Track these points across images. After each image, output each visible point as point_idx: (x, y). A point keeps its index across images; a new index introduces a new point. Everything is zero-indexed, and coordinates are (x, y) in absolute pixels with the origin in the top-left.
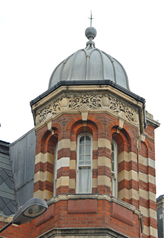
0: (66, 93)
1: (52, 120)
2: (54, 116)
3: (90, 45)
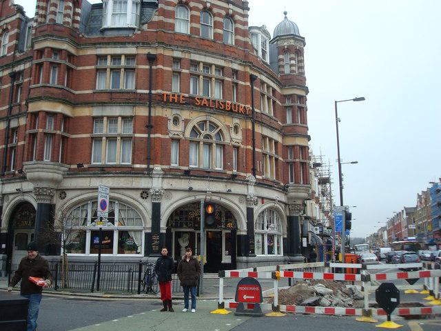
0: (293, 38)
3: (286, 18)
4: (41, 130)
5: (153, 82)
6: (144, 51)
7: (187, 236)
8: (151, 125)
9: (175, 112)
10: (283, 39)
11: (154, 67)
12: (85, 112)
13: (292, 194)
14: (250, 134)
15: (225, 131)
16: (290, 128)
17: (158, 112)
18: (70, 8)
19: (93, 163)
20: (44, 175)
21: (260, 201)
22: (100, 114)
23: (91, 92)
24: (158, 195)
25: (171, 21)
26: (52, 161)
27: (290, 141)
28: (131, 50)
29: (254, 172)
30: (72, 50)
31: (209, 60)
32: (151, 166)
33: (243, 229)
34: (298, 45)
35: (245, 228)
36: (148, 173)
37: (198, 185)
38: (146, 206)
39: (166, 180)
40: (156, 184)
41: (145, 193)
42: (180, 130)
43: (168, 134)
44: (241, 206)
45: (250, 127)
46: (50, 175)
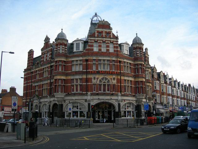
4: (57, 84)
8: (87, 80)
9: (94, 76)
11: (88, 63)
12: (70, 77)
13: (138, 97)
14: (119, 80)
15: (110, 80)
18: (63, 48)
19: (72, 92)
20: (59, 96)
21: (123, 101)
22: (73, 78)
24: (89, 101)
25: (92, 48)
26: (61, 92)
27: (137, 80)
28: (81, 58)
29: (121, 92)
30: (65, 60)
31: (105, 58)
32: (87, 93)
33: (117, 110)
34: (140, 46)
35: (118, 109)
36: (86, 94)
37: (101, 97)
38: (86, 104)
39: (92, 97)
40: (89, 98)
41: (86, 100)
44: (94, 102)
45: (119, 78)
46: (61, 96)
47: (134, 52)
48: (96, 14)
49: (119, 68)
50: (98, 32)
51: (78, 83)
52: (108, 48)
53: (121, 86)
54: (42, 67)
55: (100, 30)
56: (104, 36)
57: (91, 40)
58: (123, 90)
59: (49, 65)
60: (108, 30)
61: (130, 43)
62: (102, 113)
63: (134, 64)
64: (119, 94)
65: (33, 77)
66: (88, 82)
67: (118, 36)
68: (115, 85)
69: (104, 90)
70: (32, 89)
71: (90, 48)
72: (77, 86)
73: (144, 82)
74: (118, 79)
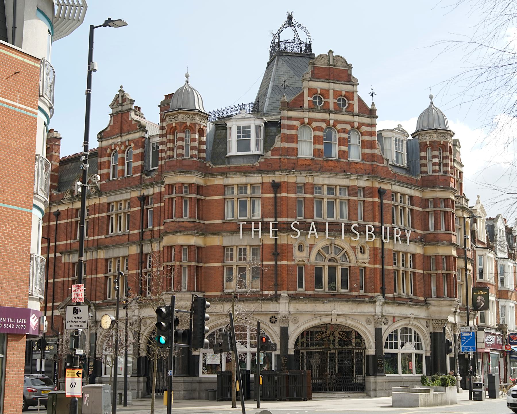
0: (436, 133)
1: (429, 141)
2: (430, 140)
5: (279, 210)
6: (268, 179)
7: (318, 356)
10: (425, 134)
12: (215, 241)
16: (432, 236)
17: (284, 239)
19: (226, 291)
23: (220, 221)
24: (286, 319)
27: (432, 250)
32: (279, 292)
35: (373, 346)
36: (276, 298)
39: (292, 305)
41: (273, 319)
42: (305, 255)
43: (293, 260)
47: (422, 158)
48: (290, 17)
49: (378, 214)
50: (312, 92)
51: (245, 259)
52: (344, 148)
53: (386, 273)
54: (104, 200)
55: (320, 85)
56: (332, 107)
57: (289, 118)
58: (389, 286)
59: (135, 194)
60: (344, 88)
61: (411, 128)
62: (321, 358)
63: (422, 199)
64: (380, 299)
65: (61, 231)
66: (279, 256)
67: (377, 107)
68: (365, 268)
69: (332, 287)
70: (60, 273)
71: (286, 145)
72: (242, 270)
73: (455, 258)
74: (375, 249)
